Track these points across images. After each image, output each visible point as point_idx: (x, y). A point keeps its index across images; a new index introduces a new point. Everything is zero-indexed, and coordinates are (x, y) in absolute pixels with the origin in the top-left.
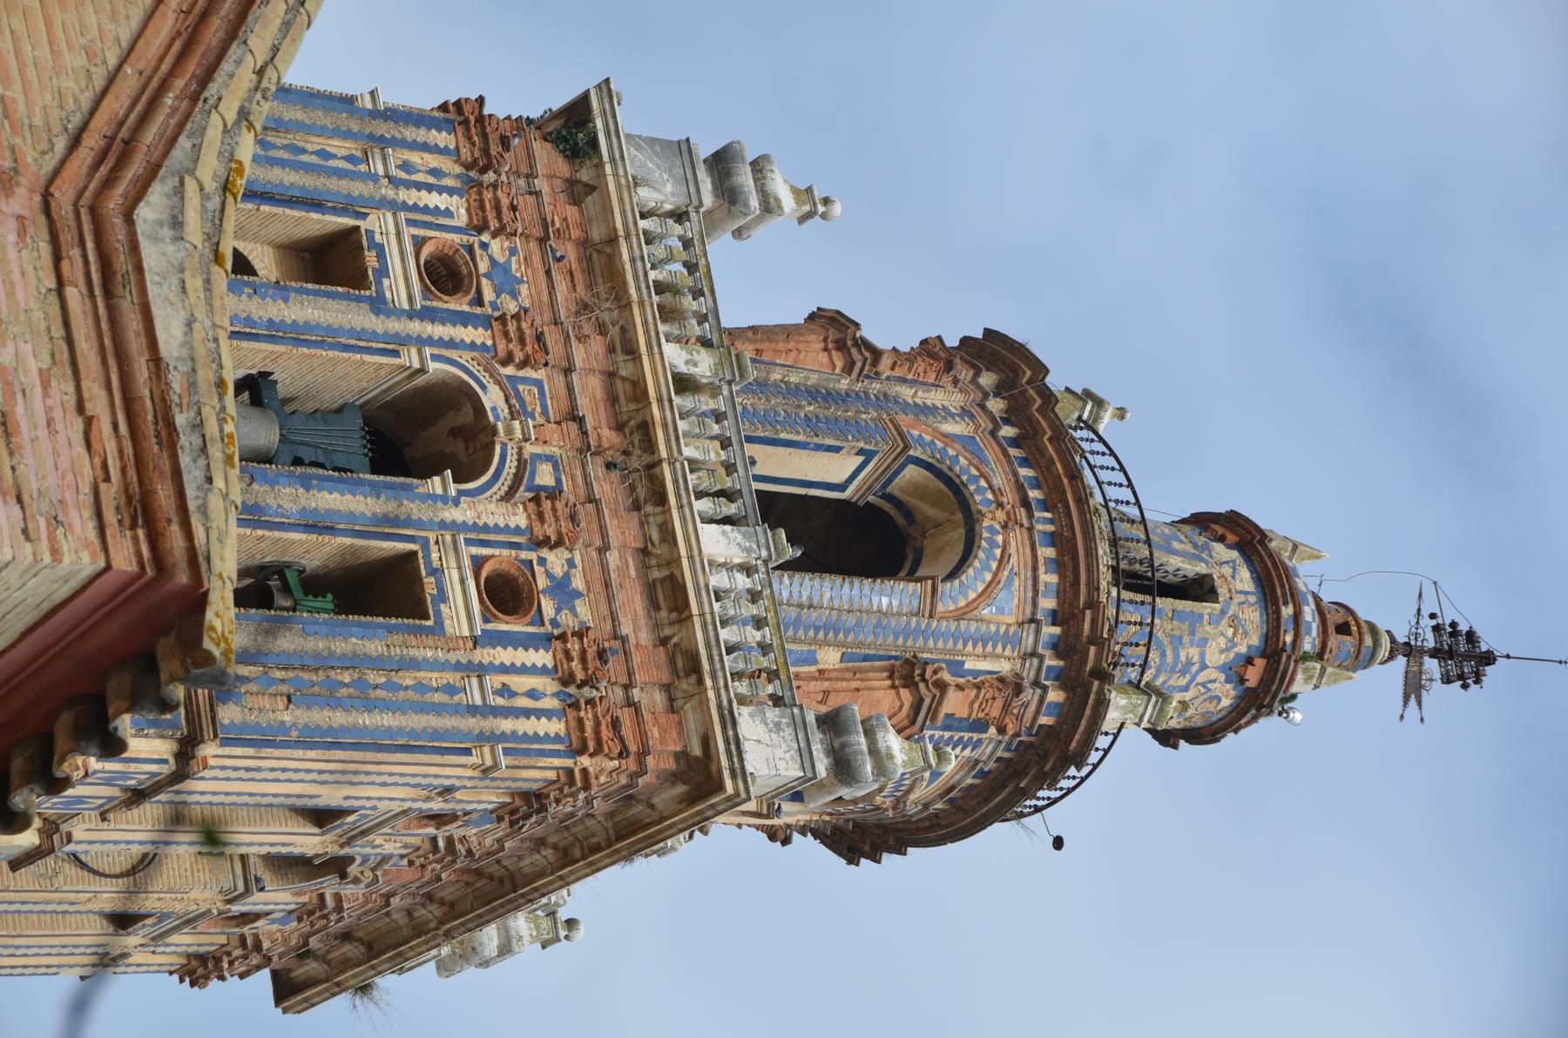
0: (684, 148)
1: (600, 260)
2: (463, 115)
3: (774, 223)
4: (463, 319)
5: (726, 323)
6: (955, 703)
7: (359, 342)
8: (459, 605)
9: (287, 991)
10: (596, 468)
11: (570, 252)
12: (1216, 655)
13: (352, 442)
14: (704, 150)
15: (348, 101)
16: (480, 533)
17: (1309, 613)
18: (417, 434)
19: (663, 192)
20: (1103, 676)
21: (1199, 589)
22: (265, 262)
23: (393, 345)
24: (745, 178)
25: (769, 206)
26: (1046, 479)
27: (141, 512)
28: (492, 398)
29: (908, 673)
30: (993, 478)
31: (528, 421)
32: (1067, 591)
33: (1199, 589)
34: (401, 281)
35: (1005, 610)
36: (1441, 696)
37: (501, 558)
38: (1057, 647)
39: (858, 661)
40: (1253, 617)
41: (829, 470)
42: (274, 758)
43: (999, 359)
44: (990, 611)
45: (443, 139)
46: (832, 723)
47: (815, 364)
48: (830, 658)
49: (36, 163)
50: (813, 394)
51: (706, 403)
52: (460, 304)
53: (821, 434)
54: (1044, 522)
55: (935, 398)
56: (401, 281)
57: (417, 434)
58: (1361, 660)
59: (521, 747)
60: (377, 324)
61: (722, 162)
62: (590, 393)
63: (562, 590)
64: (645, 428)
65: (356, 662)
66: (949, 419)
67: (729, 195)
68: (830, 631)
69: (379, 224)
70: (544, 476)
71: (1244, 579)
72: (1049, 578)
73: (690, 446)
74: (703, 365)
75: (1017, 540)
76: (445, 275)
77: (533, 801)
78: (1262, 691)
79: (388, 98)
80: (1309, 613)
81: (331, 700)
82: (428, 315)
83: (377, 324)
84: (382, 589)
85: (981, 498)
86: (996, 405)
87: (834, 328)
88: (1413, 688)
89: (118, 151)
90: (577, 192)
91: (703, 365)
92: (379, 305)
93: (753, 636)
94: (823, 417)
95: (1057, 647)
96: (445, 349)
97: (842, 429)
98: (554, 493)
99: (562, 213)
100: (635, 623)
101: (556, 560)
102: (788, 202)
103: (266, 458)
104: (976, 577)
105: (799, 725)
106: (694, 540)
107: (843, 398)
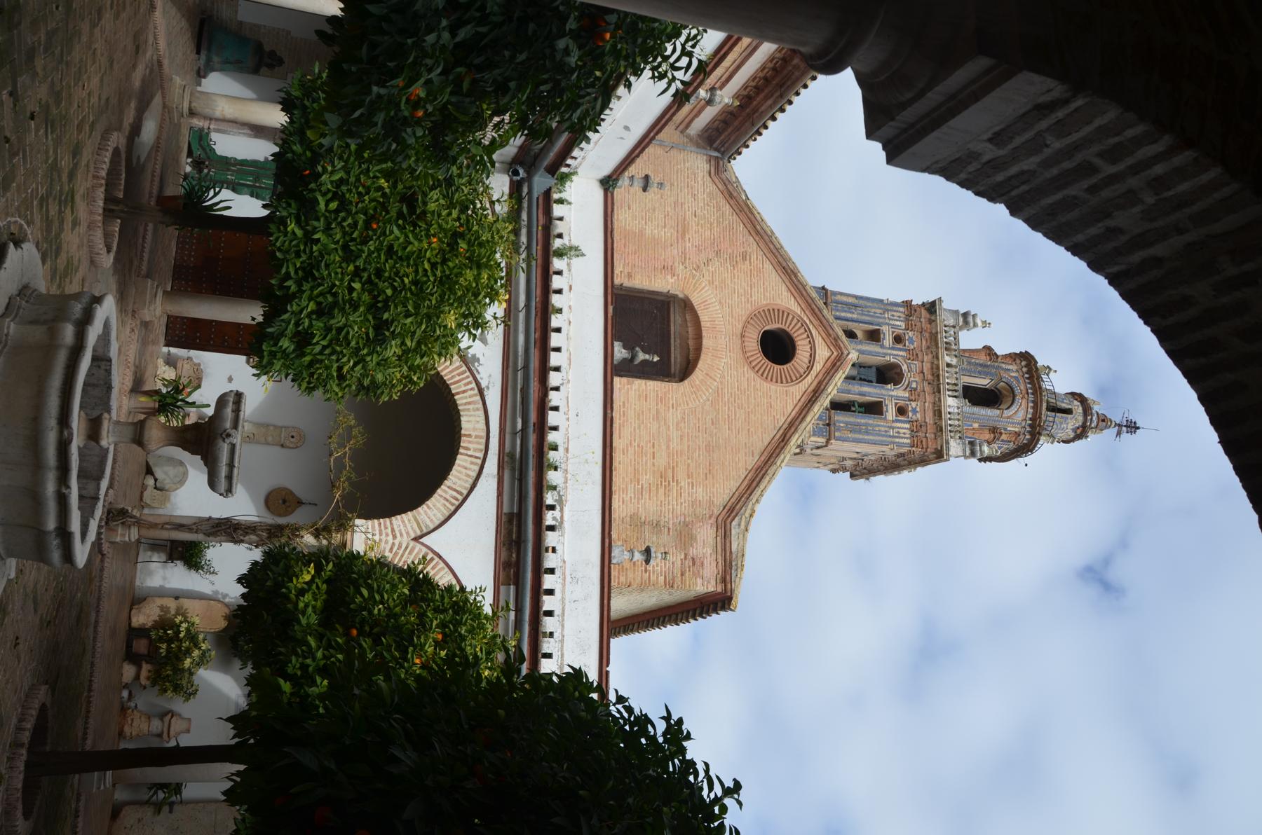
0: (957, 312)
1: (934, 337)
2: (907, 304)
3: (975, 330)
4: (900, 350)
5: (962, 347)
6: (1004, 437)
7: (877, 354)
8: (891, 413)
9: (852, 476)
10: (926, 384)
11: (927, 335)
12: (1070, 426)
13: (872, 375)
14: (962, 311)
15: (882, 301)
16: (897, 398)
17: (1095, 418)
18: (887, 375)
19: (951, 322)
20: (1040, 434)
21: (1068, 411)
22: (859, 334)
23: (884, 355)
24: (970, 319)
25: (975, 325)
26: (1034, 388)
27: (724, 581)
28: (904, 368)
29: (994, 430)
30: (1021, 387)
31: (911, 374)
32: (1034, 414)
33: (1068, 411)
34: (888, 340)
35: (1021, 415)
36: (1125, 436)
37: (901, 403)
38: (1030, 425)
39: (982, 427)
40: (1081, 419)
41: (983, 382)
42: (846, 444)
43: (1026, 359)
44: (1016, 416)
45: (902, 309)
46: (972, 443)
47: (983, 358)
48: (976, 425)
49: (716, 512)
50: (981, 365)
51: (953, 370)
52: (900, 346)
53: (982, 374)
54: (1031, 397)
55: (1010, 367)
56: (888, 340)
57: (887, 375)
58: (1106, 427)
59: (900, 445)
60: (881, 350)
61: (965, 315)
62: (927, 367)
63: (914, 411)
64: (938, 376)
65: (866, 425)
66: (1013, 372)
67: (966, 322)
68: (977, 420)
69: (885, 329)
70: (914, 385)
71: (1080, 410)
72: (1031, 411)
73: (947, 378)
74: (954, 361)
75: (1024, 401)
76: (898, 339)
77: (902, 455)
78: (1081, 433)
79: (892, 299)
80: (1095, 418)
81: (860, 432)
82: (893, 348)
83: (881, 350)
84: (874, 409)
85: (1017, 391)
86: (1025, 370)
87: (988, 350)
88: (1119, 434)
89: (732, 510)
90: (931, 322)
91: (954, 361)
92: (882, 346)
93: (957, 423)
94: (983, 370)
95: (1030, 425)
96: (894, 356)
97: (987, 374)
98: (915, 389)
99: (925, 326)
100: (930, 419)
101: (914, 404)
102: (980, 324)
103: (853, 378)
104: (1014, 409)
105: (964, 444)
106: (945, 401)
107: (986, 366)
